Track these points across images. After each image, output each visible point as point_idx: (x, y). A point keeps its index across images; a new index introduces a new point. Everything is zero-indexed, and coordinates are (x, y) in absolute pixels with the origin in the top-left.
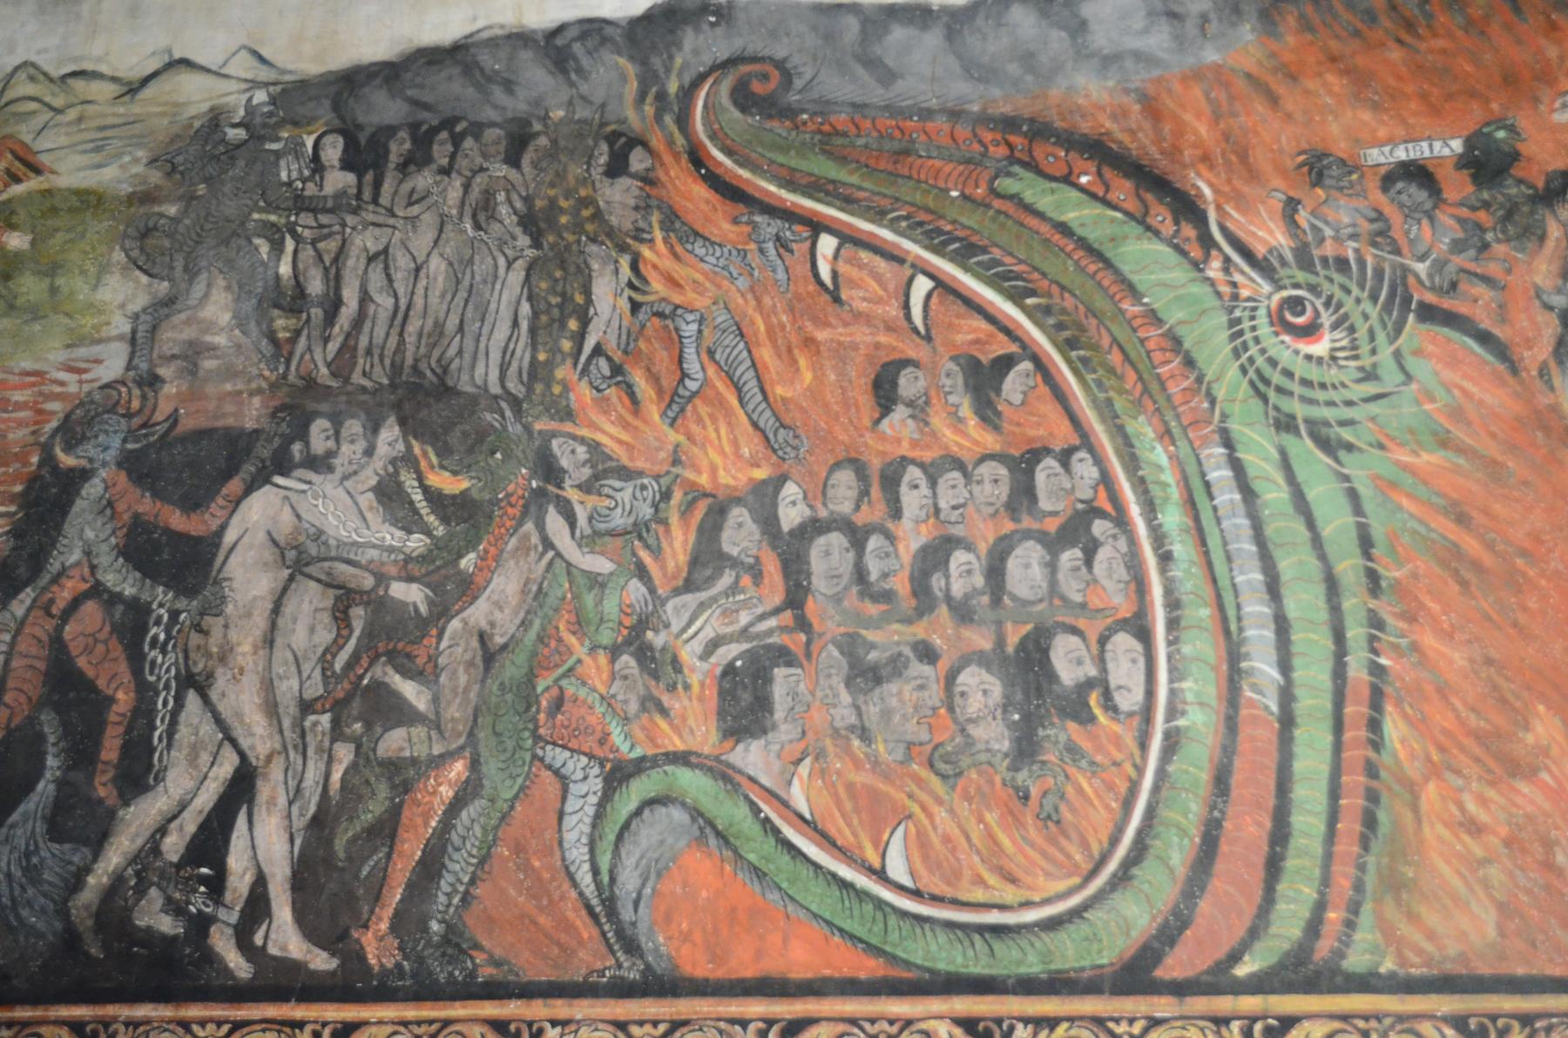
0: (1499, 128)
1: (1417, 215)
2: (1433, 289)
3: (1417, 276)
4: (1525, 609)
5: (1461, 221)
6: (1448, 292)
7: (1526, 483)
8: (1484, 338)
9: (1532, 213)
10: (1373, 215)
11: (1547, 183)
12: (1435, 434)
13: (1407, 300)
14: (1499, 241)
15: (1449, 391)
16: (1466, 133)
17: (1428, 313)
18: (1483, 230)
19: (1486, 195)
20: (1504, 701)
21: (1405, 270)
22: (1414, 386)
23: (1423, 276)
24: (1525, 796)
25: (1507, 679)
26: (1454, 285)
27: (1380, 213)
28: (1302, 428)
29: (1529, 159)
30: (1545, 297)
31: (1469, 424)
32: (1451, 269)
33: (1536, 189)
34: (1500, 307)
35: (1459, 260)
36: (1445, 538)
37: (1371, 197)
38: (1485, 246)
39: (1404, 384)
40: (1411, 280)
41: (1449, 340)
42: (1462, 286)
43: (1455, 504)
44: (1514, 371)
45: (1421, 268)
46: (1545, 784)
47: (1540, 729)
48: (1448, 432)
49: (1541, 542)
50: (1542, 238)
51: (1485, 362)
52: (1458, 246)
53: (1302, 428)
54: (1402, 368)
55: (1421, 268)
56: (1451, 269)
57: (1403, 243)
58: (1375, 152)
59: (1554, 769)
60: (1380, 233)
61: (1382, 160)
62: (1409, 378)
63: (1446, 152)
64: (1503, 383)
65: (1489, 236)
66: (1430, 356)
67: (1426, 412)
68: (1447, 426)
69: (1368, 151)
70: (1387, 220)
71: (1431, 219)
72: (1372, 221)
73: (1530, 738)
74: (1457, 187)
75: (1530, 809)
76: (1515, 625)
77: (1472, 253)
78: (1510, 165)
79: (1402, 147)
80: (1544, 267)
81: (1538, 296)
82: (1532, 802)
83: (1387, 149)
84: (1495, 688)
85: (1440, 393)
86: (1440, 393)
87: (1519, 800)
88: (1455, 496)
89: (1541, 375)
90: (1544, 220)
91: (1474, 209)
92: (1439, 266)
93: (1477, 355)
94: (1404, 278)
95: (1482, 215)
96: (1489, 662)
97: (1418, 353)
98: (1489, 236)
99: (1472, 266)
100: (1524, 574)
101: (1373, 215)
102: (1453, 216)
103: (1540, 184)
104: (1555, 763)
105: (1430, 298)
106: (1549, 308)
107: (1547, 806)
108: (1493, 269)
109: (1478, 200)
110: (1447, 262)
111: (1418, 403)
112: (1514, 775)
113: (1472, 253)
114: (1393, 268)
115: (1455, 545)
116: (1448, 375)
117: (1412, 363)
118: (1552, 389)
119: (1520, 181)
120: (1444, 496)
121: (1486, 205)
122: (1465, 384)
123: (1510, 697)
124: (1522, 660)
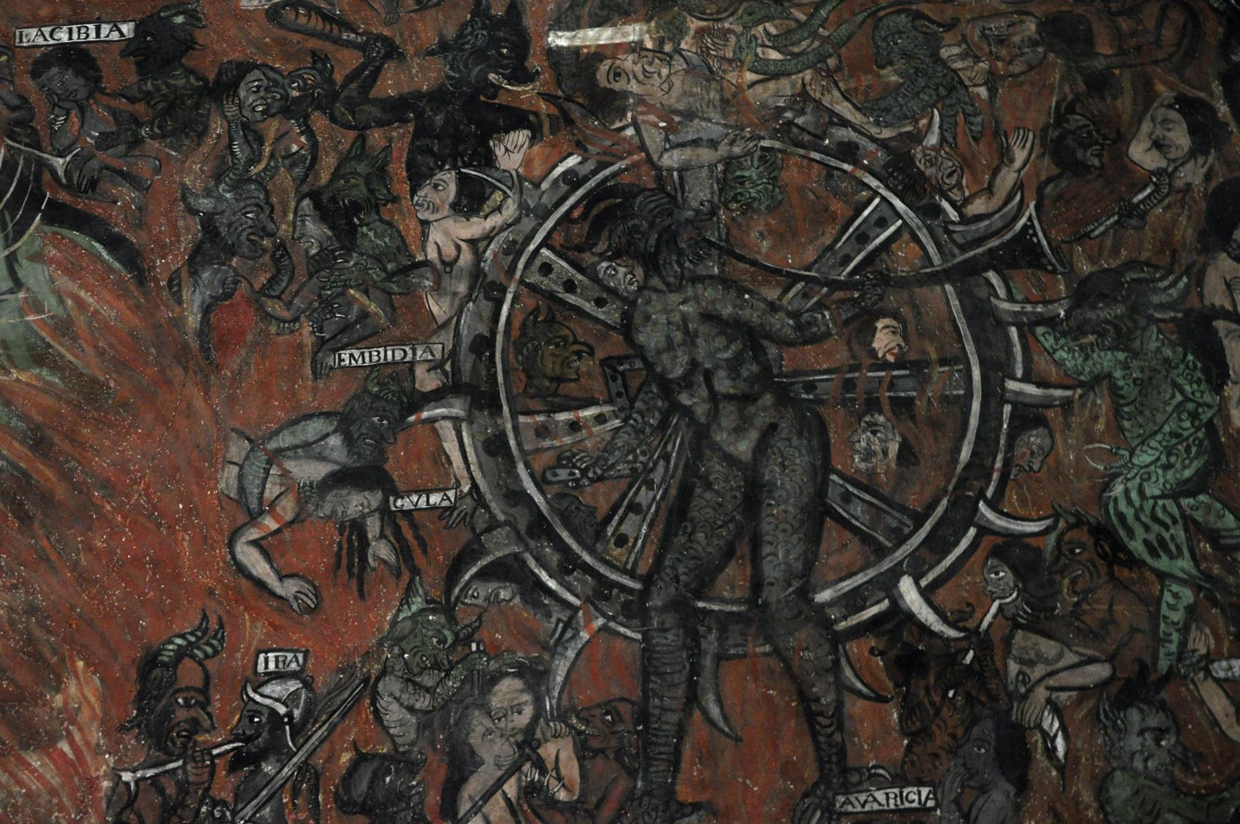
0: (177, 14)
1: (67, 105)
2: (68, 187)
3: (53, 172)
4: (90, 549)
5: (114, 113)
6: (86, 192)
7: (125, 405)
8: (115, 243)
9: (197, 106)
10: (16, 102)
11: (219, 74)
12: (31, 348)
13: (37, 198)
14: (153, 137)
15: (61, 301)
16: (140, 16)
17: (59, 215)
18: (140, 125)
19: (149, 86)
20: (37, 656)
21: (42, 164)
22: (22, 295)
23: (61, 172)
24: (34, 771)
25: (49, 631)
26: (93, 184)
27: (24, 100)
28: (12, 249)
29: (204, 47)
30: (191, 200)
31: (75, 339)
32: (94, 164)
33: (205, 80)
34: (140, 209)
35: (105, 157)
36: (17, 468)
37: (17, 81)
38: (137, 142)
39: (11, 291)
40: (47, 176)
41: (76, 245)
42: (103, 186)
43: (36, 428)
44: (141, 281)
45: (59, 163)
46: (63, 754)
47: (73, 689)
48: (49, 346)
49: (127, 472)
50: (202, 135)
51: (111, 269)
52: (105, 141)
53: (12, 249)
54: (13, 274)
55: (59, 163)
56: (94, 164)
57: (44, 134)
58: (33, 32)
59: (77, 737)
60: (19, 123)
61: (40, 41)
62: (18, 284)
63: (115, 36)
64: (124, 294)
65: (144, 132)
66: (51, 261)
67: (27, 323)
68: (48, 339)
69: (25, 31)
70: (31, 109)
71: (82, 110)
72: (13, 109)
73: (58, 700)
74: (128, 75)
75: (35, 786)
76: (75, 566)
77: (122, 148)
78: (184, 53)
79: (65, 28)
80: (197, 167)
81: (184, 199)
82: (40, 778)
83: (47, 30)
84: (30, 641)
85: (50, 302)
86: (50, 302)
87: (25, 776)
88: (39, 418)
89: (170, 285)
90: (209, 115)
91: (132, 100)
92: (80, 162)
93: (103, 262)
94: (38, 176)
95: (140, 108)
96: (32, 610)
97: (36, 257)
98: (144, 132)
99: (117, 163)
100: (99, 509)
101: (16, 102)
102: (108, 108)
103: (212, 77)
104: (81, 729)
105: (64, 197)
106: (193, 211)
107: (56, 782)
108: (143, 167)
109: (140, 90)
110: (93, 156)
111: (22, 312)
112: (25, 746)
113: (122, 148)
114: (28, 162)
115: (25, 474)
116: (64, 283)
117: (26, 270)
118: (180, 302)
119: (190, 72)
120: (24, 417)
121: (147, 97)
122: (82, 293)
123: (47, 652)
124: (72, 608)
